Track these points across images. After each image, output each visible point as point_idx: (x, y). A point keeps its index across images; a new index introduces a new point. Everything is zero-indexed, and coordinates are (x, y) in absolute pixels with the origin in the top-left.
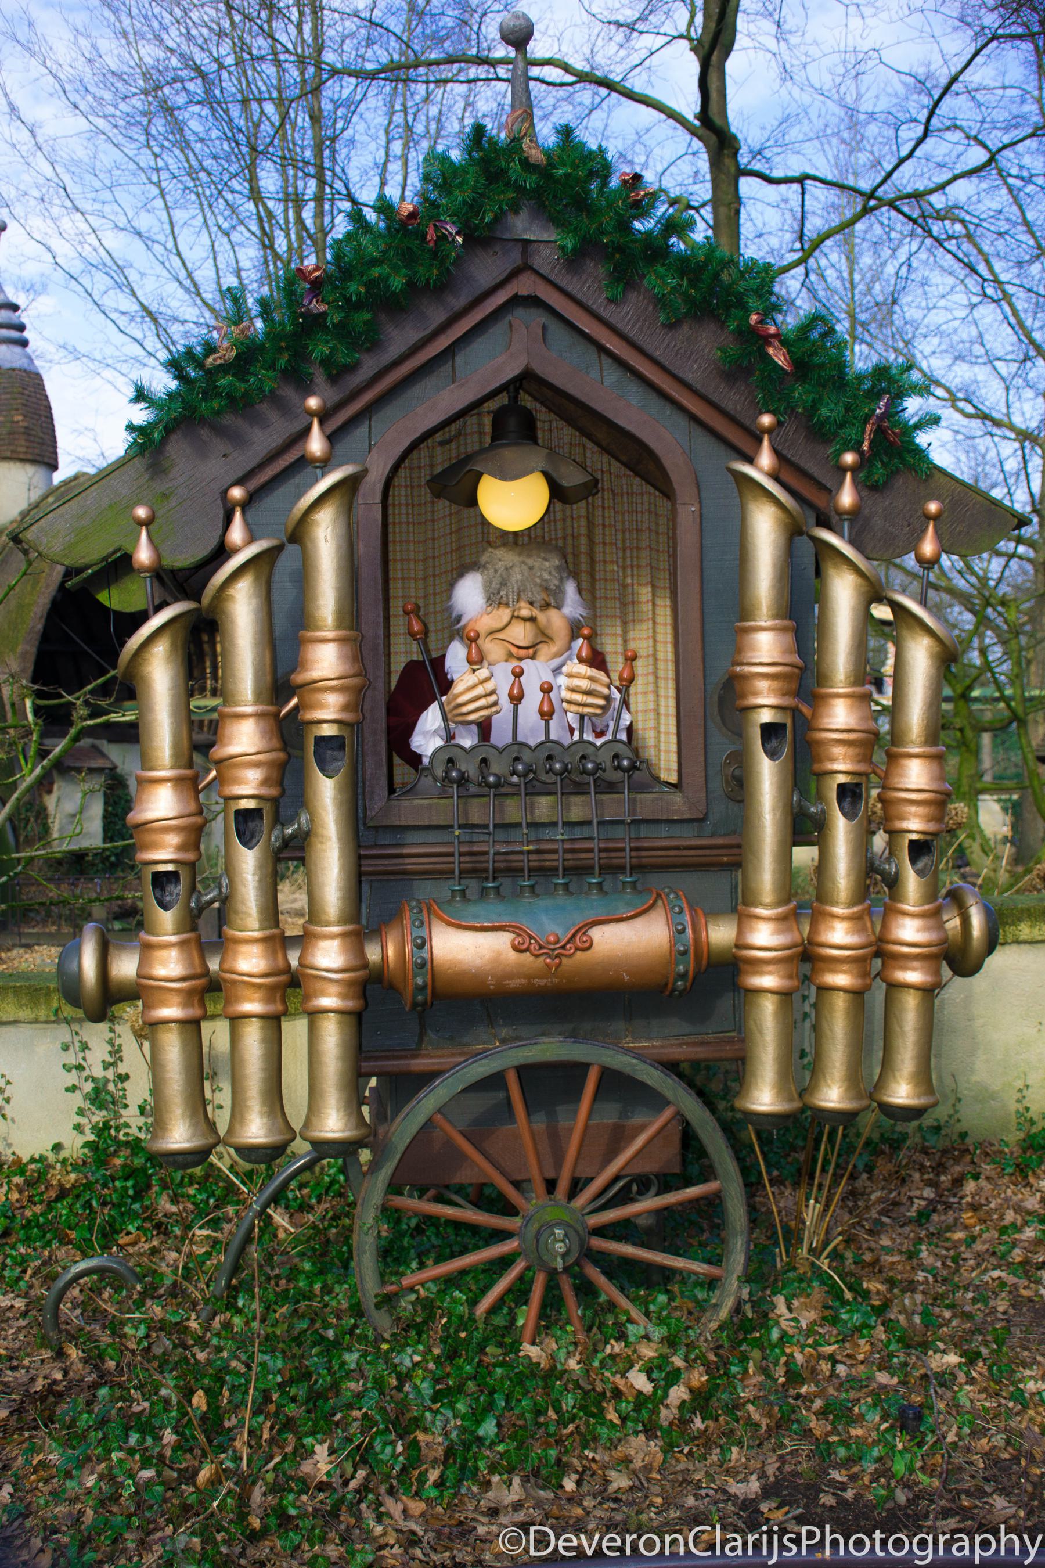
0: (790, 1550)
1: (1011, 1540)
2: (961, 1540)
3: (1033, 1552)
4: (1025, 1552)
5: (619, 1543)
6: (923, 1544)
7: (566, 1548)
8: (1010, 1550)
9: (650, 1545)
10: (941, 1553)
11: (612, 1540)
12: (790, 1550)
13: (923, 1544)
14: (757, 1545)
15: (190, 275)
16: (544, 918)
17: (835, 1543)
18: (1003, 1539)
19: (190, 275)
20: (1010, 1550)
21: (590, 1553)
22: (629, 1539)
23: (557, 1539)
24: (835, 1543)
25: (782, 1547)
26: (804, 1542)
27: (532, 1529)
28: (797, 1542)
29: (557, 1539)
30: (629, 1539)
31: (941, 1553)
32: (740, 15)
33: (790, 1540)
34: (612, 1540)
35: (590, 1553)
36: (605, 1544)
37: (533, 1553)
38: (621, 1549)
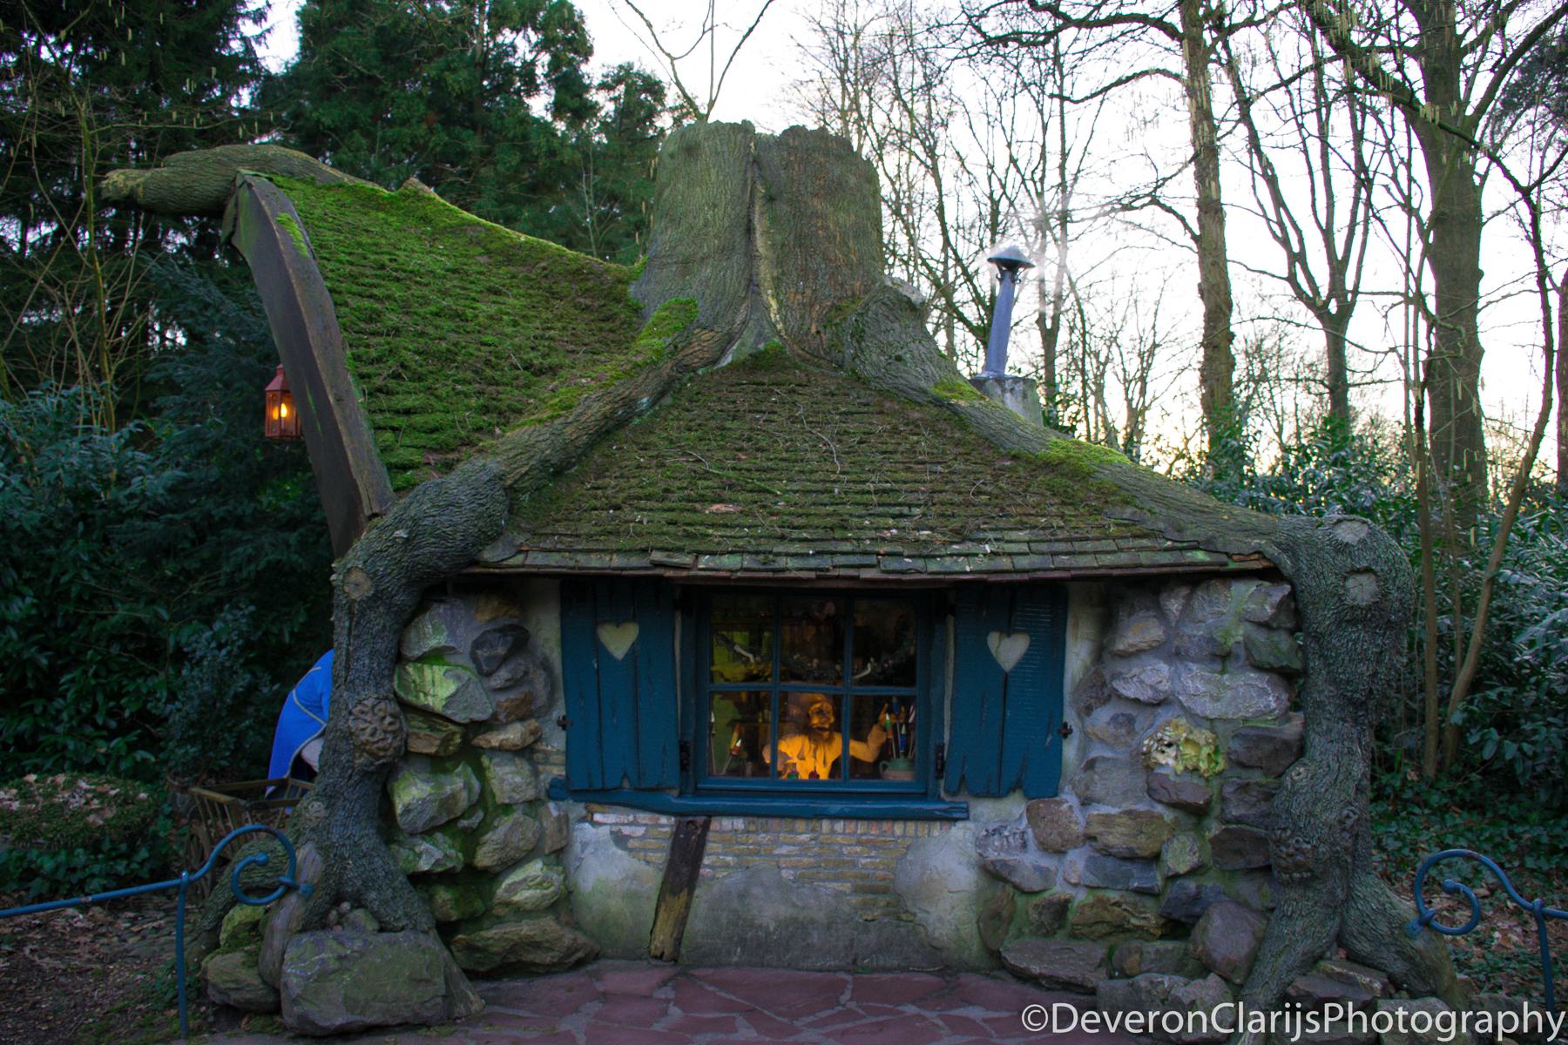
0: (1313, 1027)
1: (1534, 1017)
2: (1485, 1017)
3: (1556, 1030)
4: (1548, 1029)
5: (1142, 1020)
6: (1446, 1022)
7: (1089, 1026)
8: (1533, 1027)
9: (1173, 1022)
10: (1464, 1030)
11: (1092, 1017)
12: (1313, 1027)
13: (1446, 1022)
14: (1280, 1019)
15: (1206, 159)
16: (487, 837)
17: (1357, 1019)
18: (1526, 1016)
19: (1206, 159)
20: (1533, 1027)
21: (1112, 1030)
22: (1151, 1016)
23: (1080, 1016)
24: (1357, 1019)
25: (1305, 1023)
26: (1327, 1020)
27: (1327, 1006)
28: (1320, 1018)
29: (1080, 1016)
30: (1151, 1016)
31: (1464, 1030)
32: (1010, 345)
33: (1313, 1017)
34: (1092, 1017)
35: (1112, 1030)
36: (1128, 1021)
37: (1055, 1030)
38: (1145, 1027)
